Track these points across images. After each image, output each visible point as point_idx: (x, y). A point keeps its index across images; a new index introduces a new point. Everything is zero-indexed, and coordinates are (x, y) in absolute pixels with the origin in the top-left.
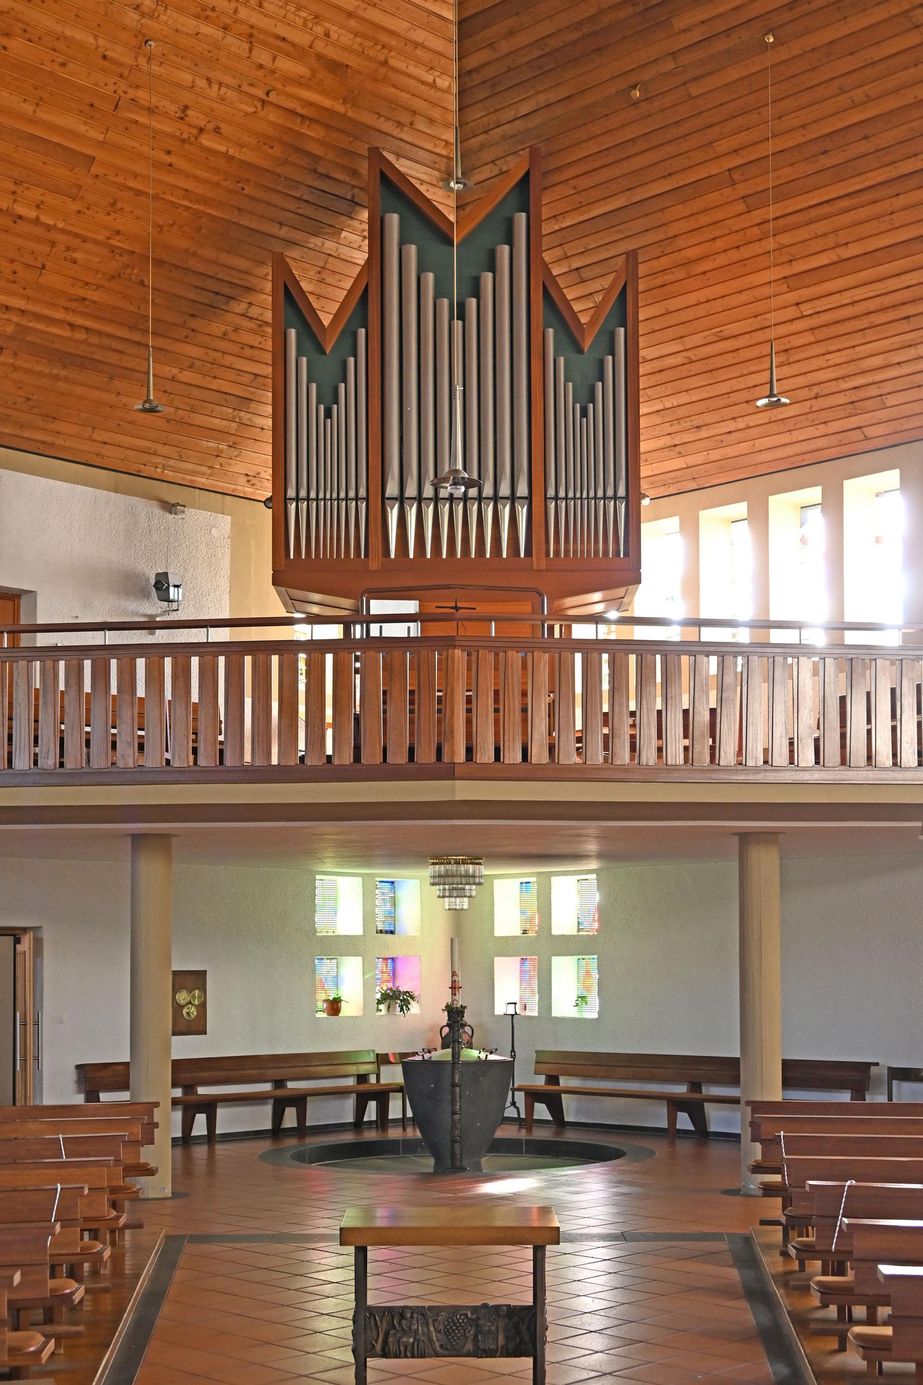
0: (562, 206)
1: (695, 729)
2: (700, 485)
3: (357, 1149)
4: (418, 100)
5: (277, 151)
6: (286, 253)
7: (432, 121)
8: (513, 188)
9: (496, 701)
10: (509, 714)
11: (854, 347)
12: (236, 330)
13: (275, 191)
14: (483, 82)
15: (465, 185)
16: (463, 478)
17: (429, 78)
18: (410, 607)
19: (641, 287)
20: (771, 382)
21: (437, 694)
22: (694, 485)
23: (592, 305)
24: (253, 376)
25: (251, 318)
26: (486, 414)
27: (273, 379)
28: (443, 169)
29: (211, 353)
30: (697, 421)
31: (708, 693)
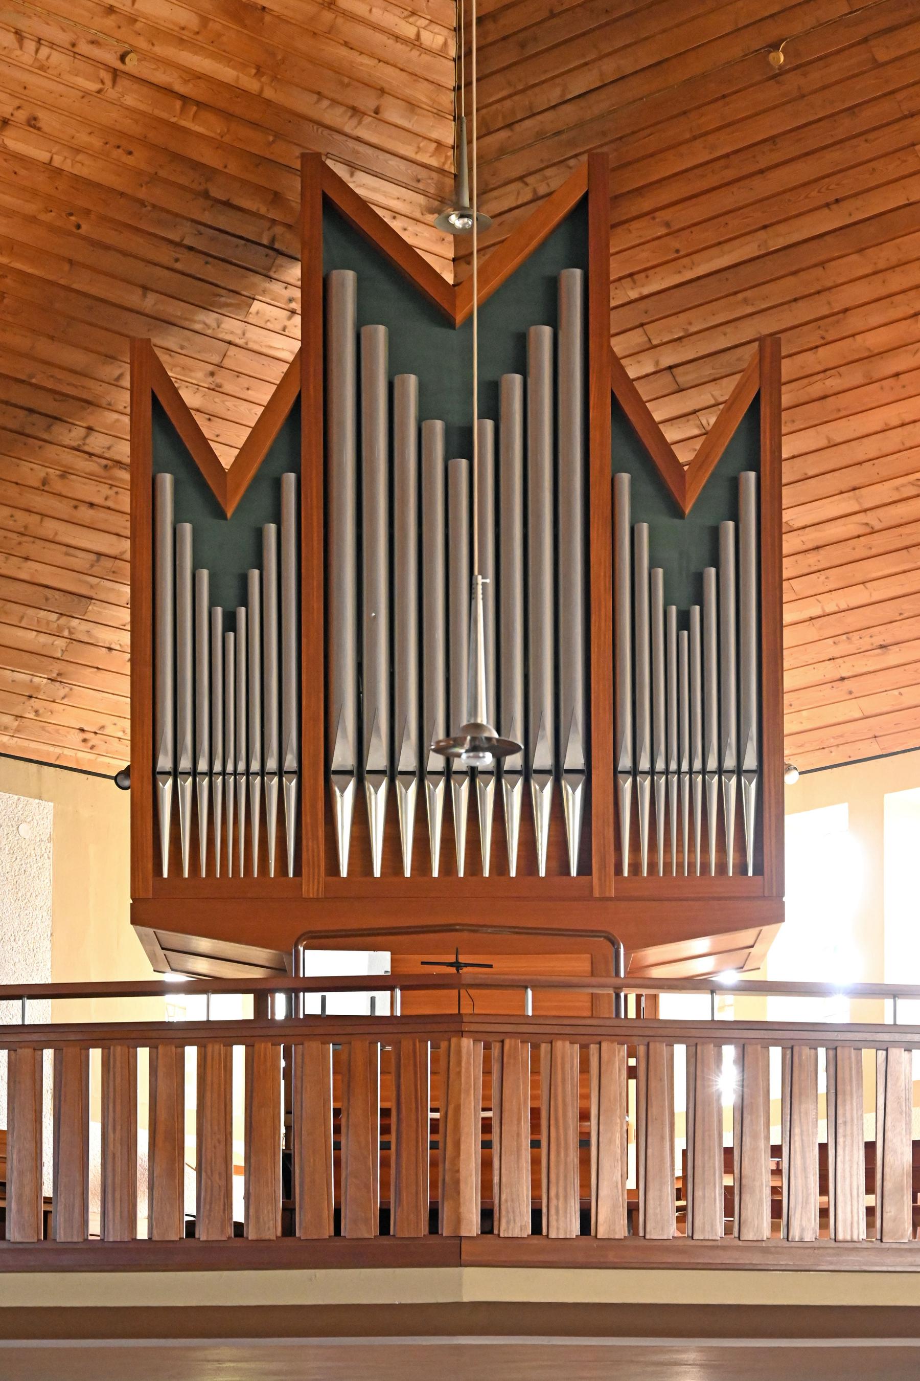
0: (645, 257)
1: (887, 1177)
4: (389, 70)
5: (139, 159)
6: (156, 340)
7: (412, 106)
8: (559, 225)
9: (535, 1127)
10: (558, 1153)
12: (64, 475)
13: (137, 230)
14: (504, 39)
16: (489, 739)
17: (409, 31)
18: (378, 963)
19: (786, 400)
21: (431, 1115)
22: (874, 749)
23: (696, 432)
24: (93, 557)
25: (91, 455)
26: (709, 628)
27: (133, 562)
28: (432, 190)
29: (19, 514)
31: (861, 1118)
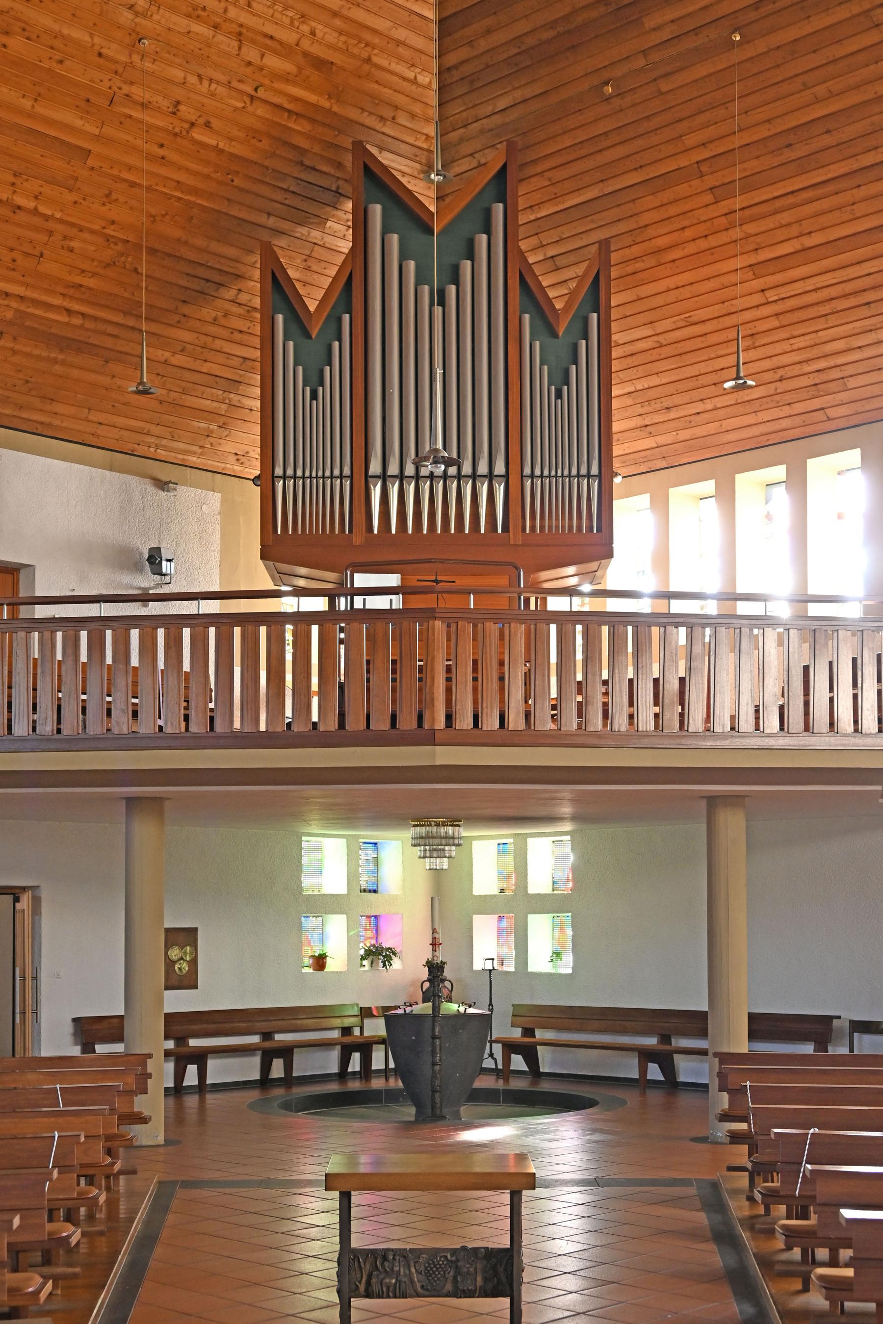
0: (537, 197)
1: (665, 697)
2: (670, 464)
3: (342, 1098)
4: (400, 96)
5: (265, 144)
6: (273, 242)
7: (413, 116)
8: (491, 180)
9: (475, 670)
10: (487, 682)
11: (817, 331)
12: (226, 315)
13: (263, 182)
14: (462, 79)
15: (445, 177)
16: (443, 457)
17: (410, 75)
18: (392, 580)
19: (613, 275)
20: (738, 366)
21: (419, 663)
22: (663, 464)
23: (567, 292)
24: (242, 360)
25: (240, 304)
26: (465, 396)
27: (261, 362)
28: (424, 161)
29: (202, 337)
30: (667, 402)
31: (677, 663)
